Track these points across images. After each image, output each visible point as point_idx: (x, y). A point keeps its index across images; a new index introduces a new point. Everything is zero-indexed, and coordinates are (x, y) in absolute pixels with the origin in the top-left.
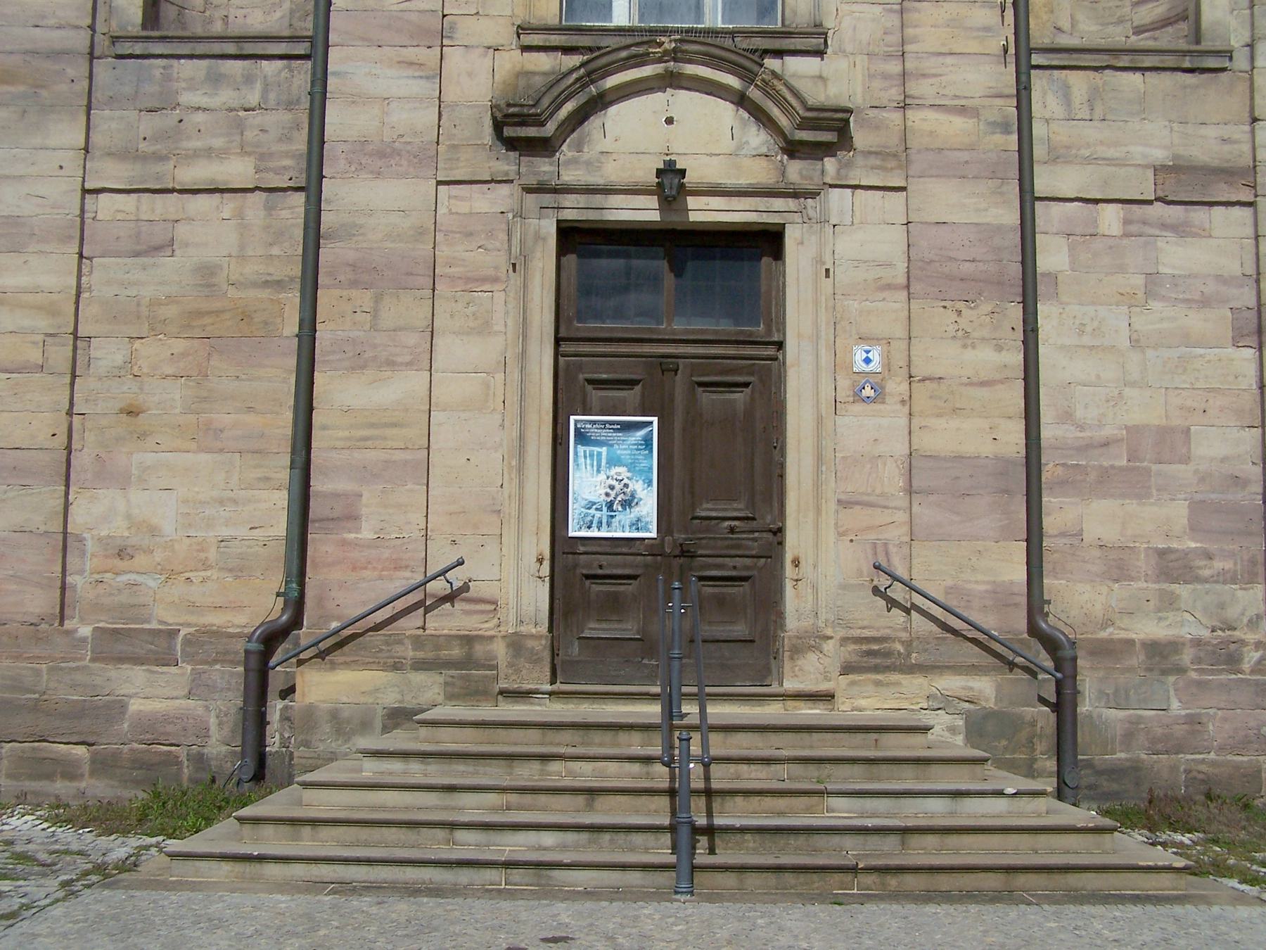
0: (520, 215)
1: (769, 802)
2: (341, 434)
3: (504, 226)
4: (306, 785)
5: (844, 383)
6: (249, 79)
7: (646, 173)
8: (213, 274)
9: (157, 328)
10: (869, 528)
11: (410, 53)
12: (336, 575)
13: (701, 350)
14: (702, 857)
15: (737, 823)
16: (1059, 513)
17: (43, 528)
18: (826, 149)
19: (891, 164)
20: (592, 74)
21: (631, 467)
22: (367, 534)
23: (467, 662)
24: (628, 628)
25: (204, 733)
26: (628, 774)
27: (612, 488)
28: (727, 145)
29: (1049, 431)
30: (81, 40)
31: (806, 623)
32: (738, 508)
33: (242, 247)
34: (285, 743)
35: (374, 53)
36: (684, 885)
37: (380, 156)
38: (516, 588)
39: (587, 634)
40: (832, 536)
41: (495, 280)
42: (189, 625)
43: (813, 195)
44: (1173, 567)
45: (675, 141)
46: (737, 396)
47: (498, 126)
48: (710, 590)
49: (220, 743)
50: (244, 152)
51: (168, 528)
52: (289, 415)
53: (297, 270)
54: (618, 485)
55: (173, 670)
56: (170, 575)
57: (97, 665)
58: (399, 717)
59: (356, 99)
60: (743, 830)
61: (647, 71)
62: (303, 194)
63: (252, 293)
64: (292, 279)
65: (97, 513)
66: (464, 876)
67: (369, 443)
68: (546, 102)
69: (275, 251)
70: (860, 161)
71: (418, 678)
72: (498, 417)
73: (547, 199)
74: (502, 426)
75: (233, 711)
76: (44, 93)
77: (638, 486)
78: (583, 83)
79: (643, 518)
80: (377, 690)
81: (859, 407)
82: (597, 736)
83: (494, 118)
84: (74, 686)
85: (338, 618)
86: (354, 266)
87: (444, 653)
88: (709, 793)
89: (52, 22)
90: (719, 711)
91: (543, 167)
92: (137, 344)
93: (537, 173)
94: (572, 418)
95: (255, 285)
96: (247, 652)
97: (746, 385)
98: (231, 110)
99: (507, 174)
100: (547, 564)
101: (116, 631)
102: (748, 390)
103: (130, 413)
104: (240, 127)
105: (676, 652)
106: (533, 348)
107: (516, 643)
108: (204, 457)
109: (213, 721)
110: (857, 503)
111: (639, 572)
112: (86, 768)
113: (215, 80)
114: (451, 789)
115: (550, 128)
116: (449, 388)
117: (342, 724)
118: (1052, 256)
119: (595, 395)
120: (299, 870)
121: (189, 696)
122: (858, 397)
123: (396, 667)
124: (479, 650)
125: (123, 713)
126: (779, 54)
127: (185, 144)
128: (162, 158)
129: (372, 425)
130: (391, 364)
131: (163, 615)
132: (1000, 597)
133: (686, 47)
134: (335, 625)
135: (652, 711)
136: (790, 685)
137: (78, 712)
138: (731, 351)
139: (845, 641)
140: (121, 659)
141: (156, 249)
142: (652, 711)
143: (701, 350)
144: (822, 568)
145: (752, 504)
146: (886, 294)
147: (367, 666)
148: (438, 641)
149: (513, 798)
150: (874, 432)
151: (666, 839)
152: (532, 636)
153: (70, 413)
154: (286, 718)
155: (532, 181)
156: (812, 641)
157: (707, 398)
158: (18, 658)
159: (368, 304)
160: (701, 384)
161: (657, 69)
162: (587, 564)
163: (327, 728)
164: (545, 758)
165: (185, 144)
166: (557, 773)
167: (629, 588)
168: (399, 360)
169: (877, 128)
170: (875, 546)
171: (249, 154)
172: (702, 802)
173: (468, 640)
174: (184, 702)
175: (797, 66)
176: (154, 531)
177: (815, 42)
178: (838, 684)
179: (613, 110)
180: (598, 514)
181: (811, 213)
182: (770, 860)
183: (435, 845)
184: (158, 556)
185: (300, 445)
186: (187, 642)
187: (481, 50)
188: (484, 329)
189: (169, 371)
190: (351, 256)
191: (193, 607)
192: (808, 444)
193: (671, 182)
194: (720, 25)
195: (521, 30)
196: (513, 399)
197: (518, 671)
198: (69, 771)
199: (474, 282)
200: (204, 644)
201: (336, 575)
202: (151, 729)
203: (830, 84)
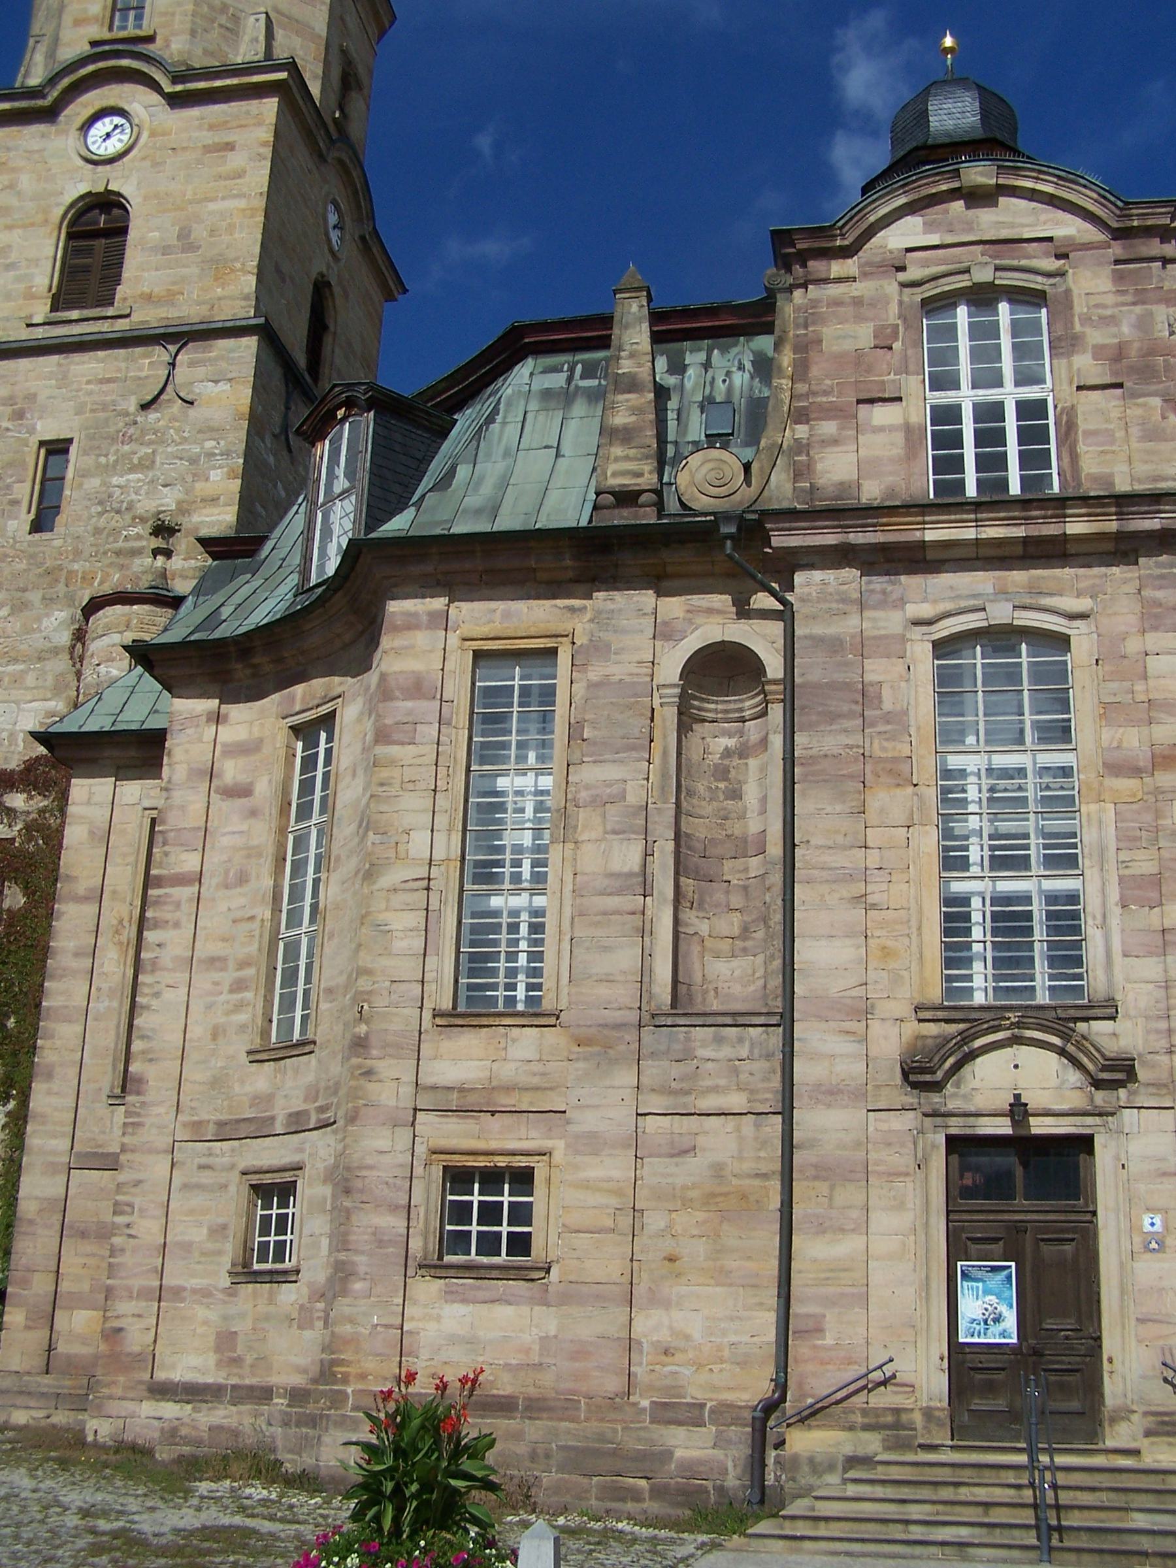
0: (921, 1132)
1: (1094, 1514)
2: (811, 1276)
3: (911, 1139)
4: (816, 1498)
5: (1137, 1239)
6: (741, 1040)
7: (1004, 1101)
8: (721, 1169)
9: (687, 1203)
10: (1160, 1337)
11: (848, 1025)
12: (810, 1367)
13: (1042, 1217)
14: (1055, 1542)
15: (1075, 1524)
17: (616, 1335)
18: (1121, 1084)
19: (1164, 1091)
20: (966, 1038)
21: (998, 1296)
22: (829, 1341)
23: (897, 1426)
24: (1000, 1404)
25: (725, 1472)
26: (1008, 1495)
27: (986, 1310)
28: (1054, 1082)
30: (633, 1017)
31: (1119, 1402)
32: (1070, 1323)
33: (740, 1151)
34: (778, 1478)
35: (824, 1025)
36: (1045, 1557)
37: (831, 1094)
38: (928, 1379)
39: (973, 1407)
40: (1134, 1343)
41: (907, 1174)
42: (712, 1400)
43: (1112, 1114)
45: (1019, 1080)
46: (1066, 1247)
47: (905, 1075)
48: (1053, 1378)
49: (734, 1479)
50: (739, 1089)
51: (697, 1335)
52: (775, 1263)
53: (778, 1166)
54: (990, 1309)
55: (704, 1429)
56: (700, 1366)
57: (655, 1426)
58: (853, 1461)
59: (815, 1056)
60: (1079, 1529)
61: (1000, 1036)
62: (780, 1116)
63: (747, 1182)
64: (774, 1173)
65: (650, 1325)
66: (918, 1550)
67: (829, 1282)
68: (936, 1059)
69: (762, 1154)
70: (1142, 1090)
71: (866, 1436)
72: (911, 1264)
73: (939, 1120)
74: (915, 1271)
75: (743, 1457)
76: (610, 1051)
77: (1003, 1309)
78: (959, 1045)
79: (1007, 1330)
80: (839, 1444)
81: (1148, 1256)
82: (987, 1472)
83: (903, 1069)
84: (639, 1440)
85: (812, 1396)
86: (816, 1166)
87: (882, 1420)
88: (1058, 1507)
89: (615, 1005)
90: (1060, 1460)
91: (936, 1098)
92: (674, 1215)
93: (930, 1104)
94: (959, 1263)
95: (749, 1176)
96: (753, 1418)
97: (1073, 1240)
98: (730, 1060)
99: (912, 1104)
100: (946, 1360)
101: (665, 1403)
102: (1074, 1243)
103: (670, 1260)
104: (736, 1072)
105: (1033, 1420)
106: (933, 1220)
107: (928, 1413)
108: (718, 1289)
109: (730, 1464)
110: (1150, 1320)
111: (1006, 1365)
112: (647, 1496)
113: (719, 1041)
114: (904, 1501)
115: (939, 1075)
116: (880, 1245)
117: (817, 1466)
119: (973, 1247)
120: (823, 1545)
121: (714, 1446)
122: (1147, 1249)
123: (851, 1428)
124: (904, 1417)
125: (672, 1458)
126: (1086, 1019)
127: (701, 1083)
128: (687, 1093)
129: (832, 1270)
130: (842, 1230)
131: (694, 1394)
133: (1025, 1020)
134: (810, 1401)
135: (1023, 1459)
136: (1110, 1443)
137: (642, 1457)
138: (1062, 1217)
139: (1146, 1414)
140: (670, 1422)
141: (686, 1152)
142: (1023, 1459)
143: (1042, 1217)
145: (1079, 1320)
146: (1164, 1179)
147: (832, 1428)
148: (877, 1412)
149: (940, 1508)
151: (1034, 1533)
152: (938, 1409)
153: (632, 1260)
154: (777, 1462)
155: (928, 1109)
156: (1122, 1414)
157: (1045, 1248)
158: (602, 1420)
159: (826, 1192)
160: (1043, 1240)
161: (1008, 1034)
162: (973, 1360)
163: (806, 1469)
164: (957, 1485)
165: (701, 1083)
166: (964, 1493)
167: (1000, 1377)
168: (847, 1227)
169: (1153, 1067)
170: (1163, 1349)
171: (744, 1090)
172: (1054, 1513)
173: (897, 1411)
174: (710, 1451)
175: (1099, 1028)
176: (687, 1337)
177: (1109, 1010)
178: (1143, 1444)
179: (979, 1060)
180: (978, 1327)
181: (1111, 1126)
182: (1096, 1546)
183: (897, 1532)
184: (691, 1354)
185: (784, 1283)
186: (712, 1411)
187: (891, 1022)
188: (901, 1206)
189: (695, 1232)
190: (814, 1160)
191: (714, 1389)
192: (1115, 1282)
193: (1018, 1110)
194: (1047, 1001)
195: (917, 1009)
196: (921, 1253)
197: (929, 1432)
198: (636, 1496)
199: (894, 1175)
200: (724, 1413)
201: (810, 1367)
202: (690, 1469)
203: (1120, 1038)
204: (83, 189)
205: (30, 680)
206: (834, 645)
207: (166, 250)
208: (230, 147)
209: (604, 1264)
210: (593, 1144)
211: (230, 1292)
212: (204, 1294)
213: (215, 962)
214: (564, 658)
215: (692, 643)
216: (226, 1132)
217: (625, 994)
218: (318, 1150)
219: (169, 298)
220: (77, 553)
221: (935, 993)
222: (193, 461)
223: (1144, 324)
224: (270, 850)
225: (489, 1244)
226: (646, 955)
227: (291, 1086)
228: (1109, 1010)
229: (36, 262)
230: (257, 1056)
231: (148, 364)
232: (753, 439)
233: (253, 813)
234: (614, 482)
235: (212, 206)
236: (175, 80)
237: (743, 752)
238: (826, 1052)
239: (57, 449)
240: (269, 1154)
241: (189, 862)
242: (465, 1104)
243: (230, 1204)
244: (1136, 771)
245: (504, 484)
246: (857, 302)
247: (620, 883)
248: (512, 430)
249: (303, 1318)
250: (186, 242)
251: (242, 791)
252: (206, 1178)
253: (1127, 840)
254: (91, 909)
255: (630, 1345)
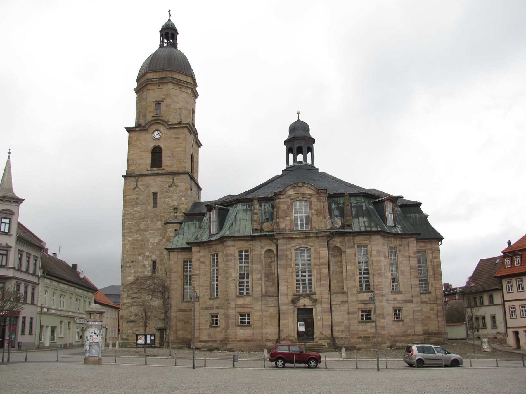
16: (334, 328)
20: (299, 297)
29: (333, 322)
44: (343, 332)
45: (305, 302)
54: (302, 329)
118: (333, 309)
131: (269, 338)
132: (329, 335)
144: (317, 333)
150: (320, 323)
177: (315, 294)
193: (304, 305)
202: (270, 346)
204: (153, 145)
205: (156, 234)
206: (283, 250)
207: (170, 157)
208: (179, 138)
209: (258, 324)
210: (257, 311)
211: (209, 329)
212: (205, 329)
213: (202, 286)
214: (249, 251)
215: (265, 249)
216: (207, 308)
217: (259, 293)
218: (221, 312)
219: (171, 166)
220: (161, 212)
221: (295, 292)
222: (179, 197)
223: (320, 206)
224: (209, 271)
225: (245, 323)
226: (262, 288)
227: (216, 303)
228: (315, 294)
229: (146, 158)
230: (210, 299)
231: (169, 179)
232: (272, 220)
233: (206, 266)
234: (255, 228)
235: (177, 149)
236: (169, 125)
237: (272, 262)
238: (283, 299)
239: (155, 194)
240: (214, 311)
241: (197, 272)
242: (241, 306)
243: (208, 318)
244: (318, 265)
245: (240, 226)
246: (285, 202)
247: (258, 280)
248: (240, 216)
249: (221, 332)
250: (173, 156)
251: (204, 263)
252: (204, 314)
253: (317, 274)
254: (176, 274)
255: (262, 333)
